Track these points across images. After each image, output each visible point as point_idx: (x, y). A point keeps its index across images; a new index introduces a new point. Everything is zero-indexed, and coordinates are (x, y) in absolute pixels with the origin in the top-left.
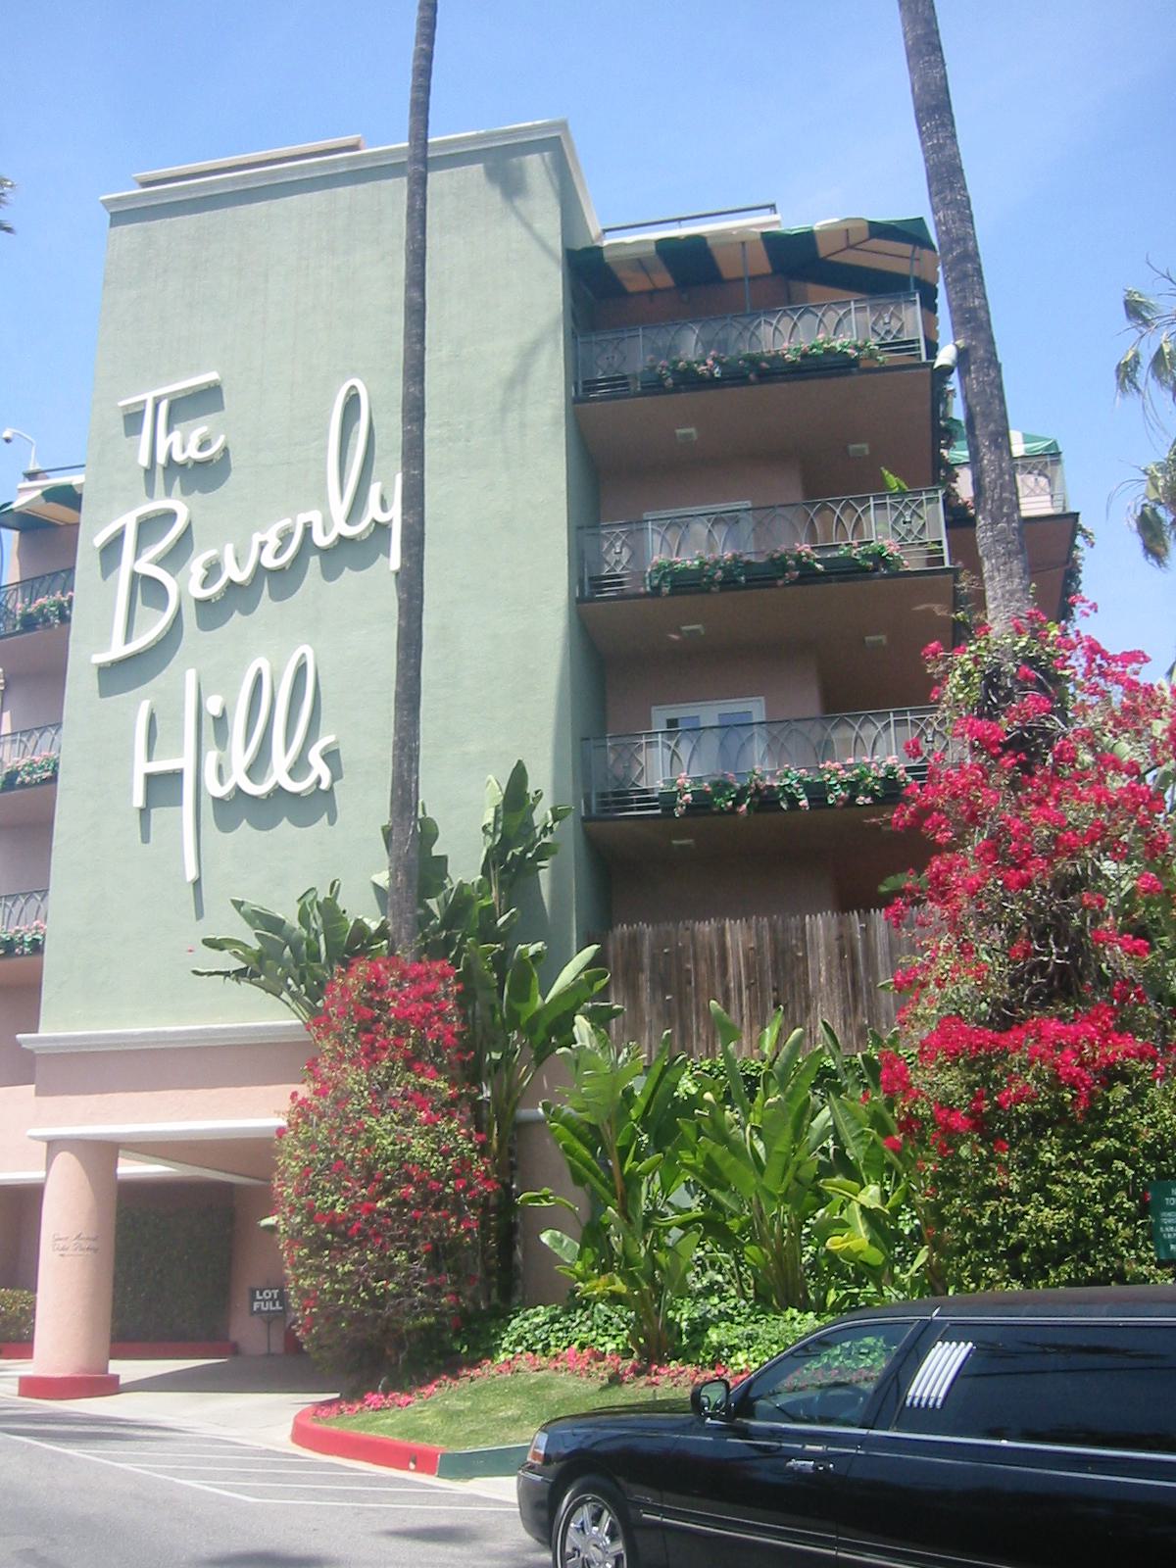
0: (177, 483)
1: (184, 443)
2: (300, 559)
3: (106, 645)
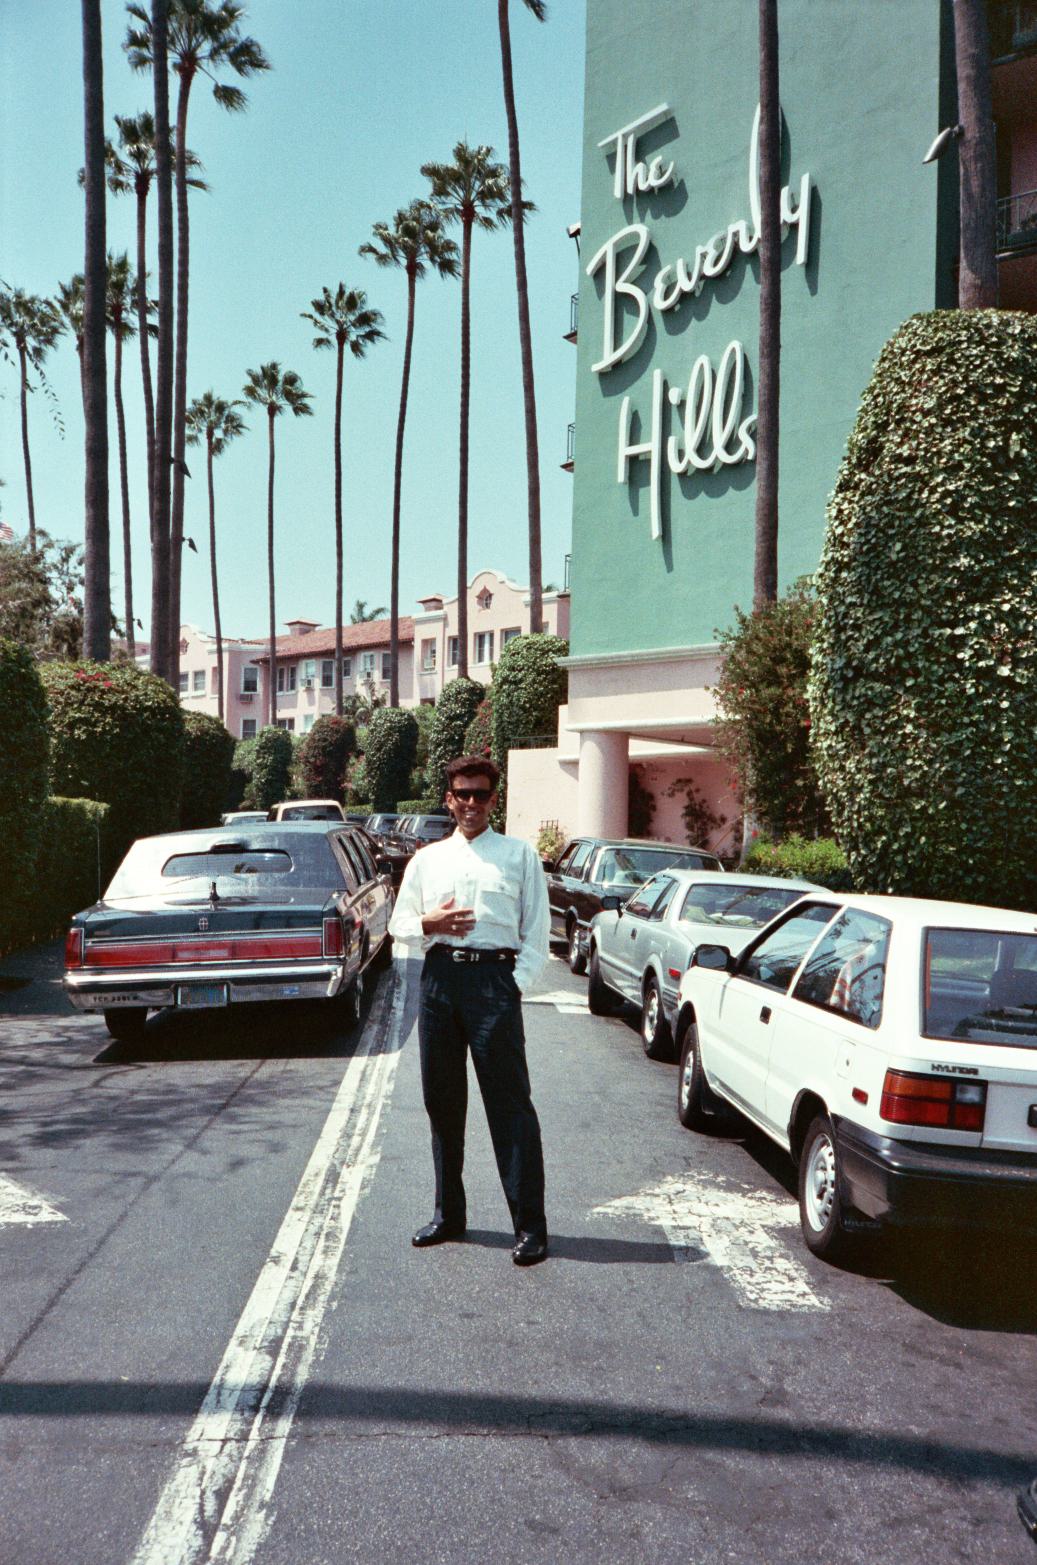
0: (649, 212)
1: (646, 175)
2: (730, 265)
3: (599, 357)
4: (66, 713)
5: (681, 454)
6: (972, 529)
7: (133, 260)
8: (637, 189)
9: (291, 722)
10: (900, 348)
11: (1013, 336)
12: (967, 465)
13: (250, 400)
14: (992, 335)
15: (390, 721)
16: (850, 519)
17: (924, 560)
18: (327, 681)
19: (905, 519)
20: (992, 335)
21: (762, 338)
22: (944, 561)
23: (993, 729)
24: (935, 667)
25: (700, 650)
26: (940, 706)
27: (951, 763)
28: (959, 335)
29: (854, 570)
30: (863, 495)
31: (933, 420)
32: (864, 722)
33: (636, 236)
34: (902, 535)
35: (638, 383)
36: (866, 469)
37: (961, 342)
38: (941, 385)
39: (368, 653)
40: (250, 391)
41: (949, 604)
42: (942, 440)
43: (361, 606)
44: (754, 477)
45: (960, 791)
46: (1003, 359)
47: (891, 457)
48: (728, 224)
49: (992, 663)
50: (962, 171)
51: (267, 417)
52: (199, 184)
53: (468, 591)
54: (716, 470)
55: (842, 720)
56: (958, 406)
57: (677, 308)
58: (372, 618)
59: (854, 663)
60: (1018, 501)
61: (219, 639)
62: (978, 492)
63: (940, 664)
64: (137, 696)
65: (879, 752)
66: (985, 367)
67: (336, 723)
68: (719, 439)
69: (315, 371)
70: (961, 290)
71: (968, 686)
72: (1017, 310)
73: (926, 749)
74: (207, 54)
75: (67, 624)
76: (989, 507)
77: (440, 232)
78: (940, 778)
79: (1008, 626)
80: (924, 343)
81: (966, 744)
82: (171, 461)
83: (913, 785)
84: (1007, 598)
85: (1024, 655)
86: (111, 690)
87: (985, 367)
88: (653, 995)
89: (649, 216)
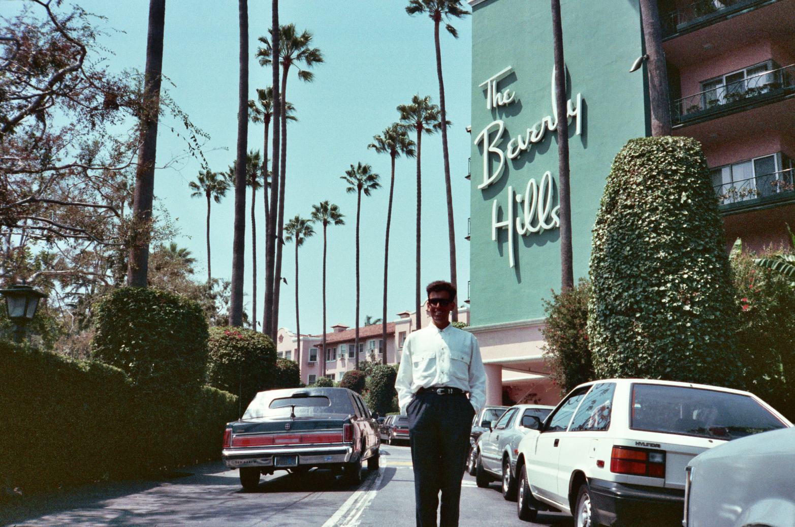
1: (502, 98)
2: (544, 136)
3: (482, 182)
4: (219, 351)
5: (523, 226)
6: (665, 238)
7: (262, 154)
8: (498, 105)
9: (333, 376)
10: (623, 155)
11: (680, 147)
12: (661, 208)
13: (314, 219)
14: (669, 147)
15: (383, 372)
16: (603, 238)
17: (642, 254)
18: (351, 355)
19: (631, 235)
20: (669, 147)
21: (560, 168)
22: (652, 254)
23: (683, 337)
24: (651, 307)
25: (536, 321)
26: (654, 326)
27: (663, 355)
28: (652, 148)
29: (607, 261)
30: (609, 226)
31: (642, 188)
32: (616, 336)
33: (498, 125)
34: (630, 242)
35: (501, 193)
36: (609, 213)
37: (653, 151)
38: (644, 171)
39: (372, 340)
40: (315, 215)
41: (656, 275)
42: (647, 196)
43: (369, 318)
44: (559, 236)
45: (668, 370)
46: (675, 158)
47: (622, 206)
48: (542, 118)
49: (680, 304)
50: (649, 75)
51: (323, 227)
52: (293, 118)
53: (421, 308)
54: (541, 233)
55: (605, 336)
56: (654, 181)
57: (519, 157)
58: (374, 323)
59: (609, 307)
60: (688, 225)
61: (298, 335)
62: (667, 221)
63: (653, 305)
64: (254, 343)
65: (624, 351)
66: (667, 161)
67: (355, 374)
68: (542, 217)
69: (346, 204)
70: (653, 129)
71: (669, 316)
72: (682, 136)
73: (649, 348)
74: (296, 57)
75: (224, 318)
76: (674, 227)
77: (406, 137)
78: (657, 362)
79: (687, 285)
80: (635, 152)
81: (670, 346)
82: (276, 237)
83: (643, 367)
84: (686, 272)
85: (697, 300)
86: (241, 339)
87: (667, 161)
88: (508, 467)
89: (504, 116)
